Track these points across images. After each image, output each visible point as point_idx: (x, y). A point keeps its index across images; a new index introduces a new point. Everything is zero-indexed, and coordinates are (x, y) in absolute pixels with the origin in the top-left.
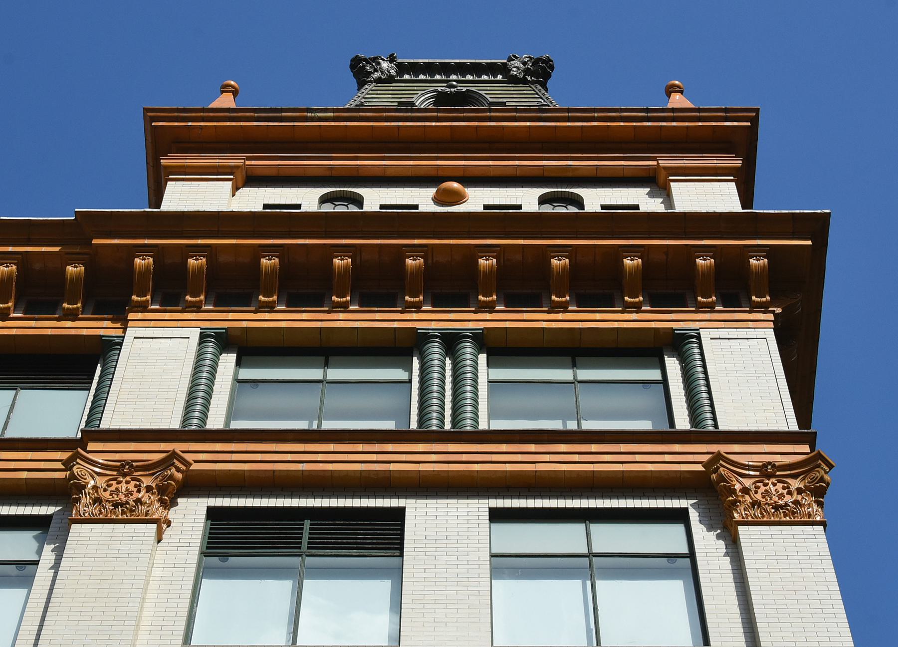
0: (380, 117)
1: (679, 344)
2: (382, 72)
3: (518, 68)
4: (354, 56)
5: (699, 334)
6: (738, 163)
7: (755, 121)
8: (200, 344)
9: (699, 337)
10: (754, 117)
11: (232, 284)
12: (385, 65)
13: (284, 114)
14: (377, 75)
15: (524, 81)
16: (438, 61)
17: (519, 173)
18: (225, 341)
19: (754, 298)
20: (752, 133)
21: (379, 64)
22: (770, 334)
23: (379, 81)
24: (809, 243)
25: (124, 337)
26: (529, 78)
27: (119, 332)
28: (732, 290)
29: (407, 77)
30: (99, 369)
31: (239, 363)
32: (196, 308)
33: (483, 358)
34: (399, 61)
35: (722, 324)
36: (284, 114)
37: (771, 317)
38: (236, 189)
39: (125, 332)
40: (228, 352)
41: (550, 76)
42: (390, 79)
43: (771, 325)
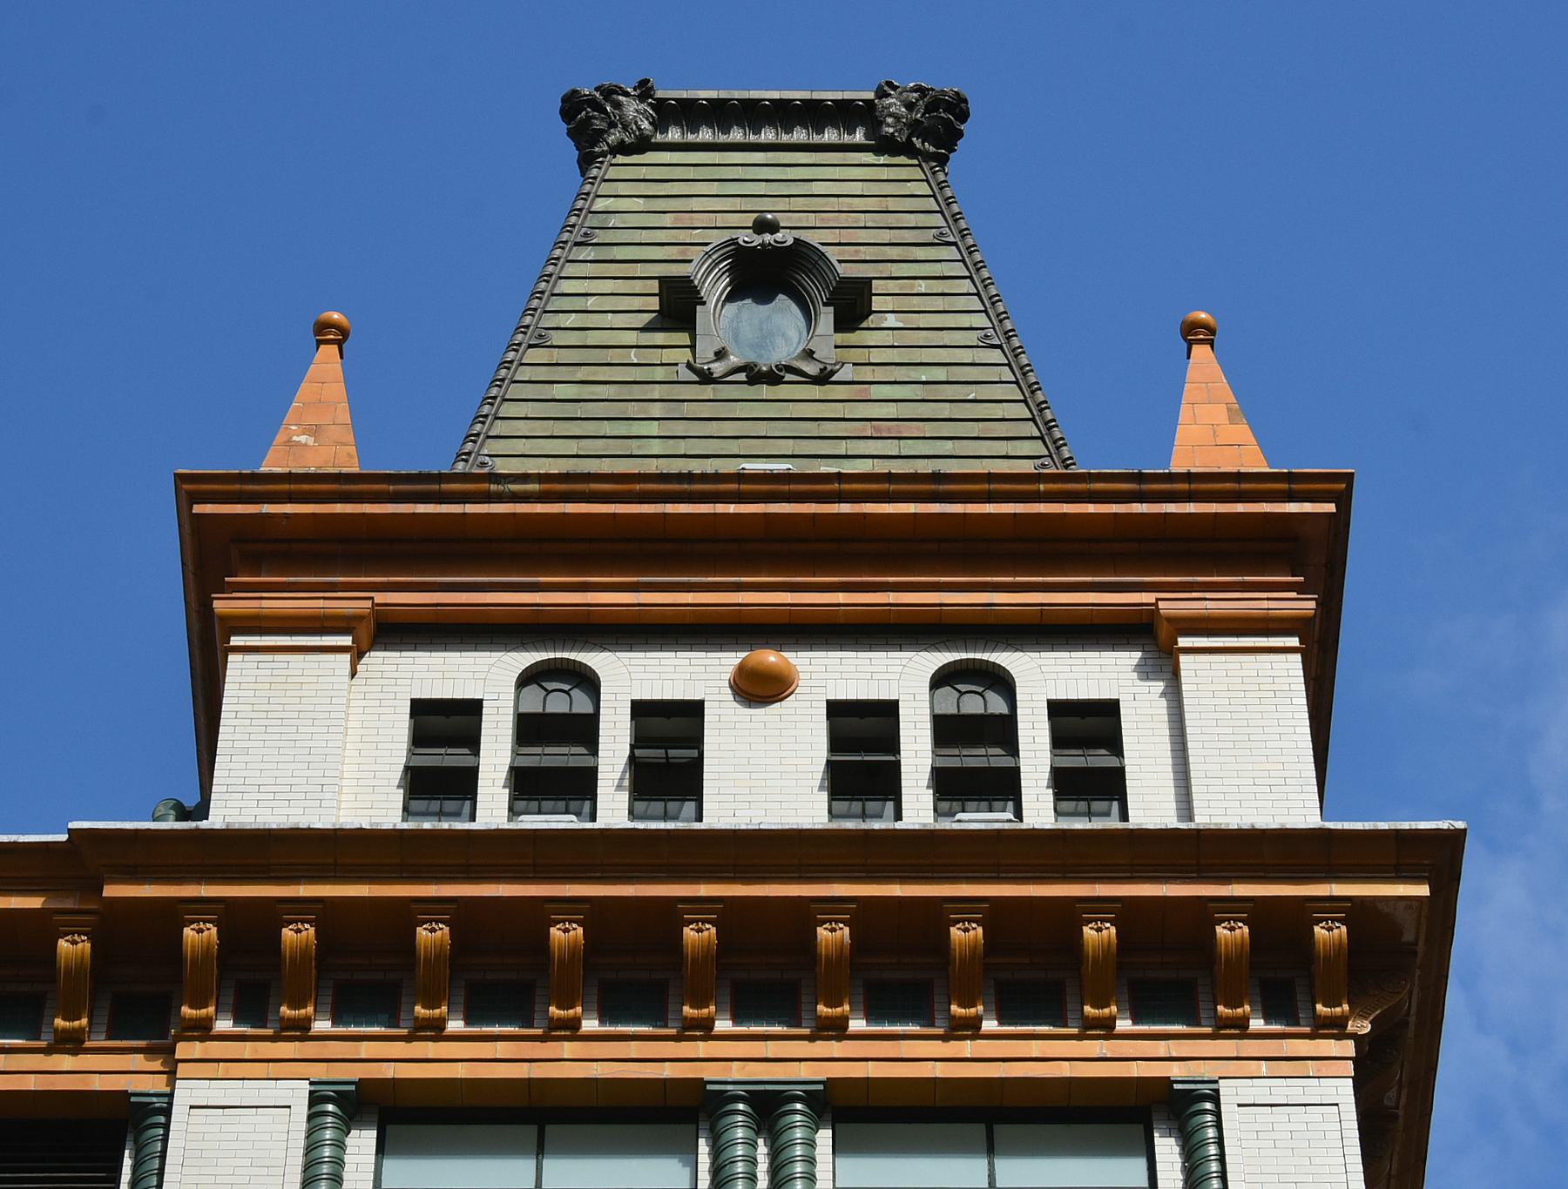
0: (630, 492)
1: (1180, 1109)
2: (625, 128)
3: (897, 117)
4: (566, 90)
5: (1217, 1091)
6: (1308, 605)
7: (1344, 501)
8: (310, 1118)
9: (1215, 1098)
10: (1339, 488)
11: (367, 972)
12: (631, 108)
13: (444, 486)
14: (614, 137)
15: (908, 149)
16: (737, 94)
17: (991, 620)
18: (358, 1104)
19: (1319, 1007)
20: (1338, 526)
21: (618, 106)
22: (1344, 1092)
23: (622, 148)
24: (1423, 890)
25: (171, 1095)
26: (917, 142)
27: (158, 1084)
28: (1281, 980)
29: (674, 135)
30: (127, 1162)
31: (381, 1150)
32: (300, 1030)
33: (824, 1137)
34: (659, 94)
35: (1264, 1067)
36: (444, 486)
37: (1348, 1047)
38: (358, 654)
39: (172, 1083)
40: (362, 1125)
41: (960, 134)
42: (643, 145)
43: (1349, 1068)
